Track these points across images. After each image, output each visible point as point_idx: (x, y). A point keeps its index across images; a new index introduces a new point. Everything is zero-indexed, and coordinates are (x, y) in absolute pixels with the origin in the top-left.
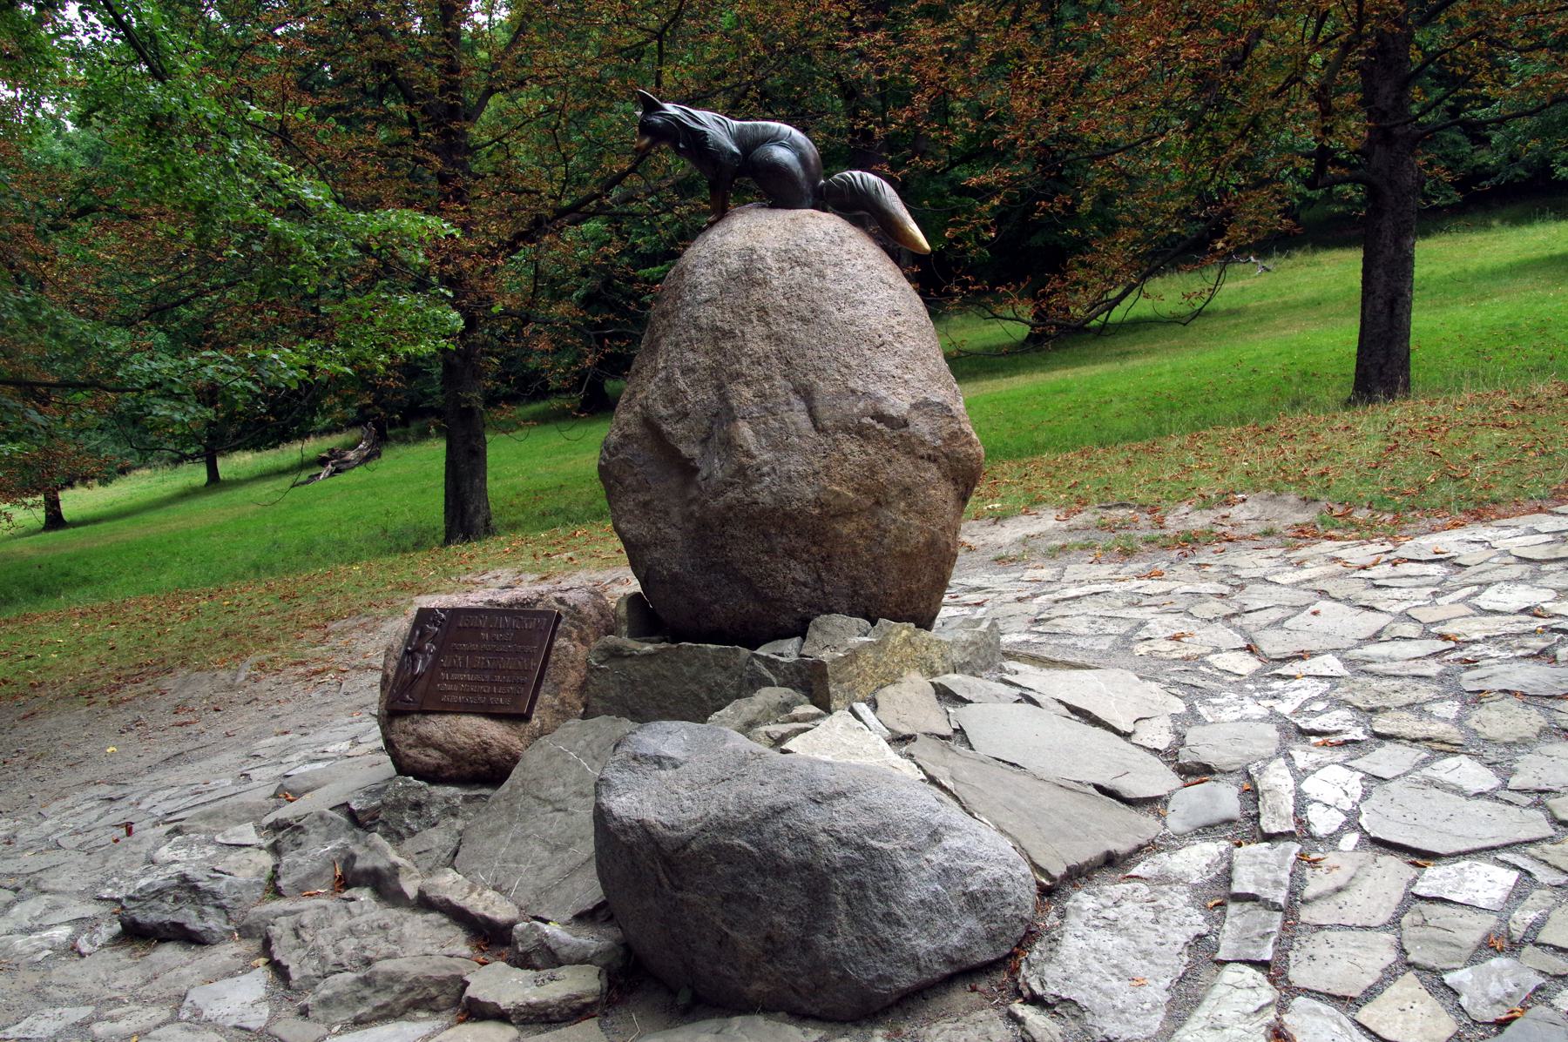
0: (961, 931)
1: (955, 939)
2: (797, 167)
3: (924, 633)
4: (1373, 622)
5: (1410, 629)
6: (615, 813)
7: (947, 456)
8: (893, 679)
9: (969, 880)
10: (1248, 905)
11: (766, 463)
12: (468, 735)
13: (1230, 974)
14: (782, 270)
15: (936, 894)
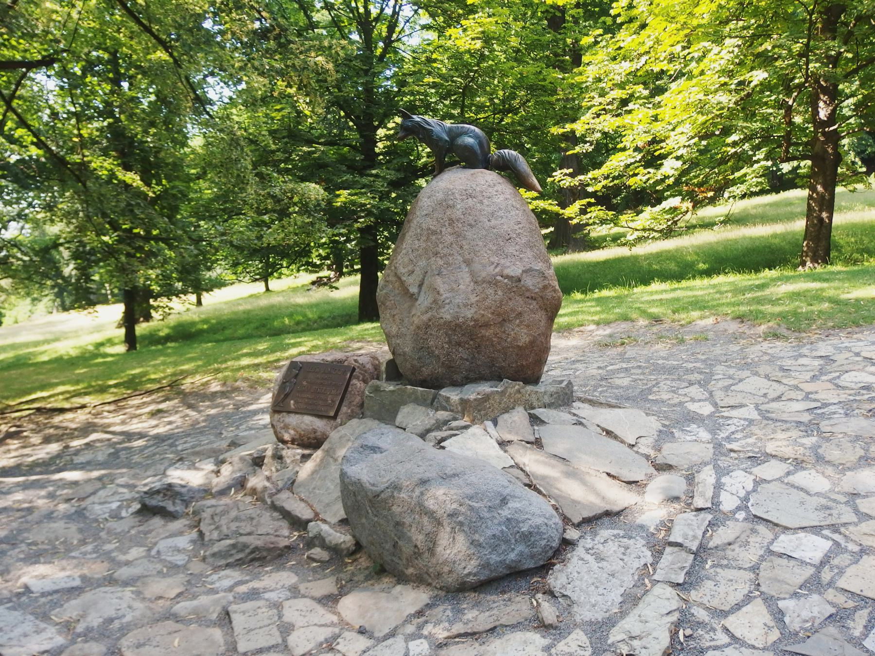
0: (516, 552)
1: (512, 556)
2: (477, 148)
3: (529, 388)
4: (780, 389)
5: (800, 395)
6: (348, 474)
7: (541, 297)
8: (507, 410)
9: (521, 525)
10: (676, 549)
11: (448, 298)
12: (307, 425)
13: (658, 590)
14: (463, 200)
15: (502, 531)
